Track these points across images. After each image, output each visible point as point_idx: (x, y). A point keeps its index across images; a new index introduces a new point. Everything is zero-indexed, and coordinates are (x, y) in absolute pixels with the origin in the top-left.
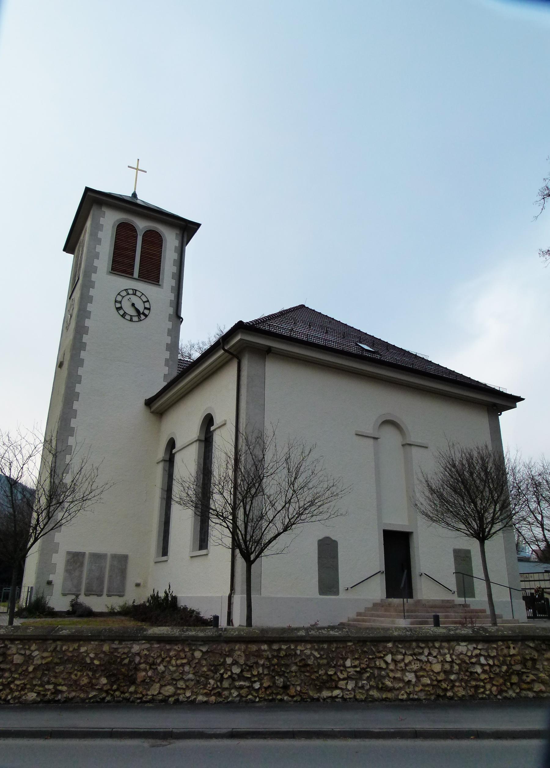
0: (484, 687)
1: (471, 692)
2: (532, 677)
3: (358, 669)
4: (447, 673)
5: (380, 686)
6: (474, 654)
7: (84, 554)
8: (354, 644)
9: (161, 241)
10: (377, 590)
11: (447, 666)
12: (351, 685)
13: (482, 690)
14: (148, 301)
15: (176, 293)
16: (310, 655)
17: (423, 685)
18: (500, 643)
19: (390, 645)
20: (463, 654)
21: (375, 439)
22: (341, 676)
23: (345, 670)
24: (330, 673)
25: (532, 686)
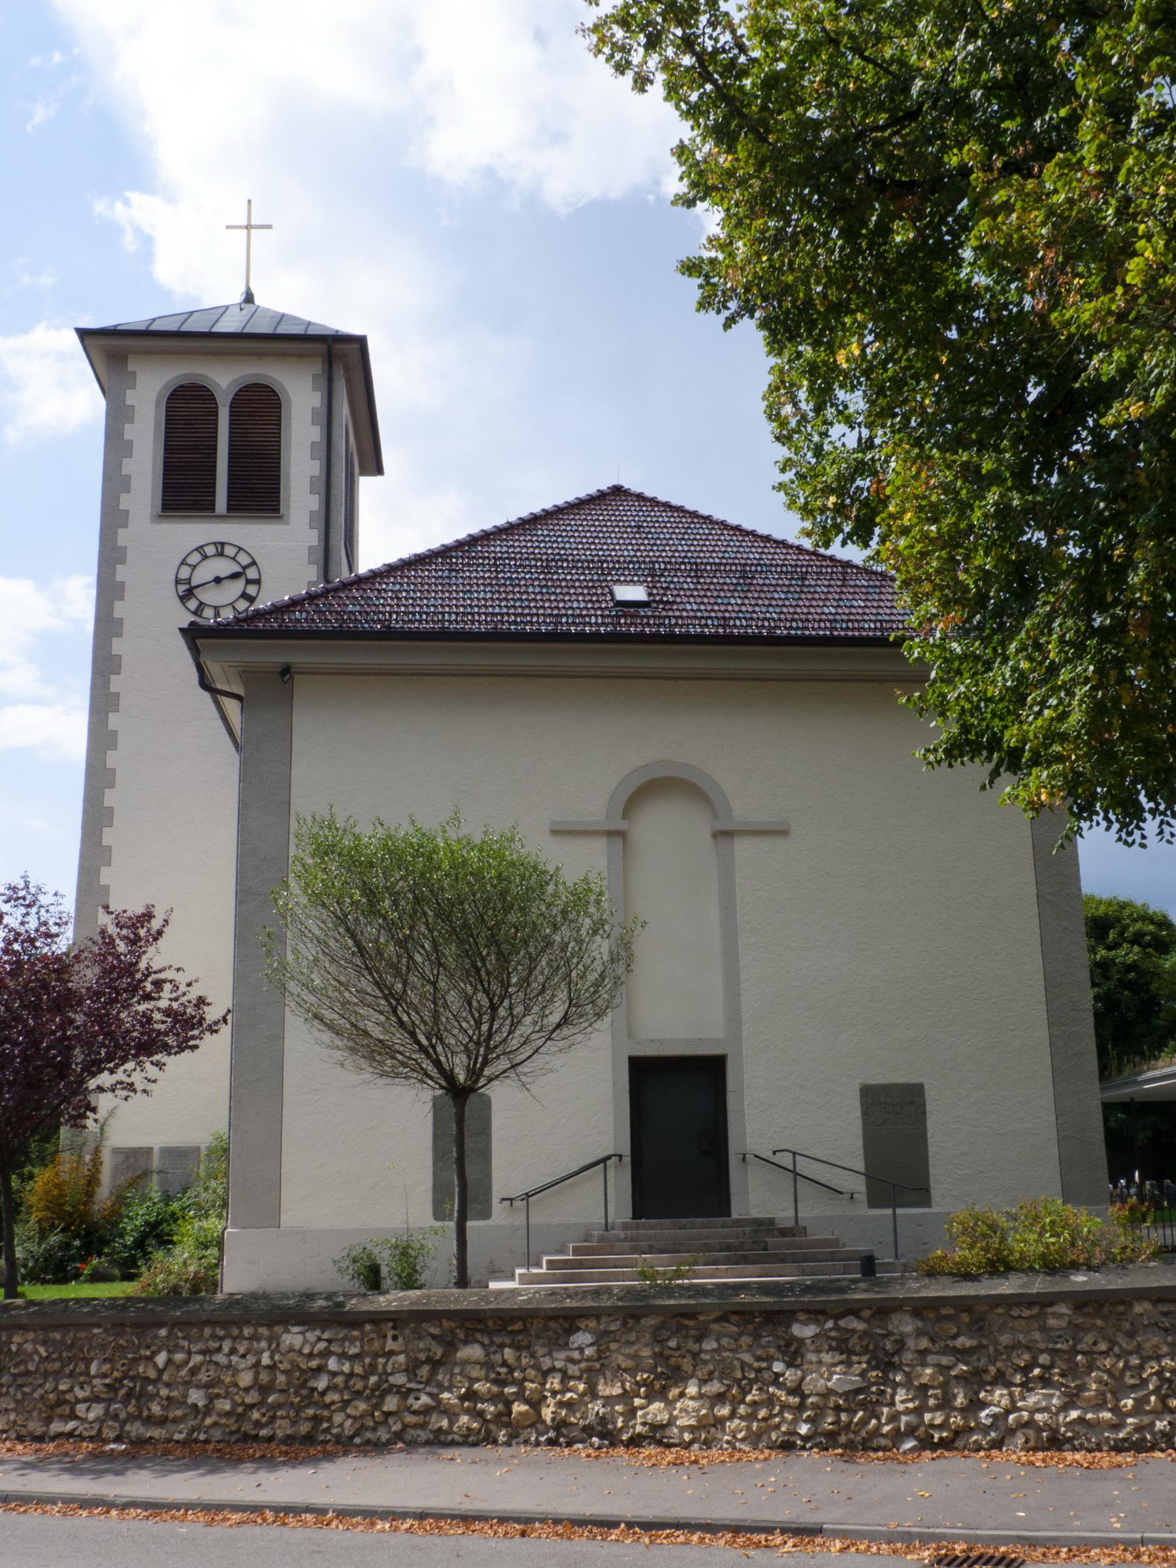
0: (330, 1419)
1: (304, 1428)
2: (425, 1399)
3: (108, 1381)
4: (265, 1390)
5: (145, 1414)
6: (315, 1352)
7: (150, 1150)
8: (106, 1330)
9: (278, 406)
10: (605, 1201)
11: (264, 1377)
12: (96, 1411)
13: (325, 1425)
14: (254, 563)
15: (323, 529)
16: (31, 1355)
17: (219, 1415)
18: (368, 1327)
19: (163, 1332)
20: (293, 1350)
21: (621, 834)
22: (80, 1394)
23: (90, 1383)
24: (62, 1387)
25: (427, 1419)
